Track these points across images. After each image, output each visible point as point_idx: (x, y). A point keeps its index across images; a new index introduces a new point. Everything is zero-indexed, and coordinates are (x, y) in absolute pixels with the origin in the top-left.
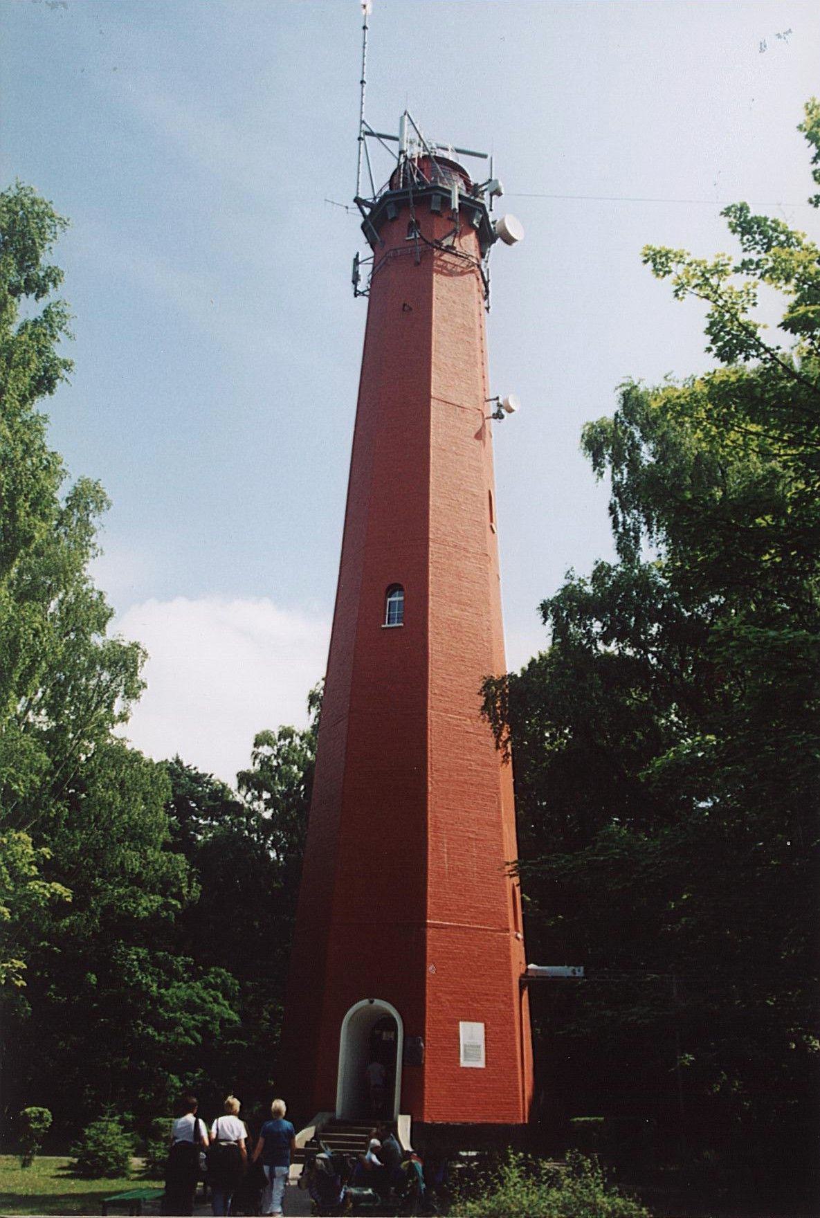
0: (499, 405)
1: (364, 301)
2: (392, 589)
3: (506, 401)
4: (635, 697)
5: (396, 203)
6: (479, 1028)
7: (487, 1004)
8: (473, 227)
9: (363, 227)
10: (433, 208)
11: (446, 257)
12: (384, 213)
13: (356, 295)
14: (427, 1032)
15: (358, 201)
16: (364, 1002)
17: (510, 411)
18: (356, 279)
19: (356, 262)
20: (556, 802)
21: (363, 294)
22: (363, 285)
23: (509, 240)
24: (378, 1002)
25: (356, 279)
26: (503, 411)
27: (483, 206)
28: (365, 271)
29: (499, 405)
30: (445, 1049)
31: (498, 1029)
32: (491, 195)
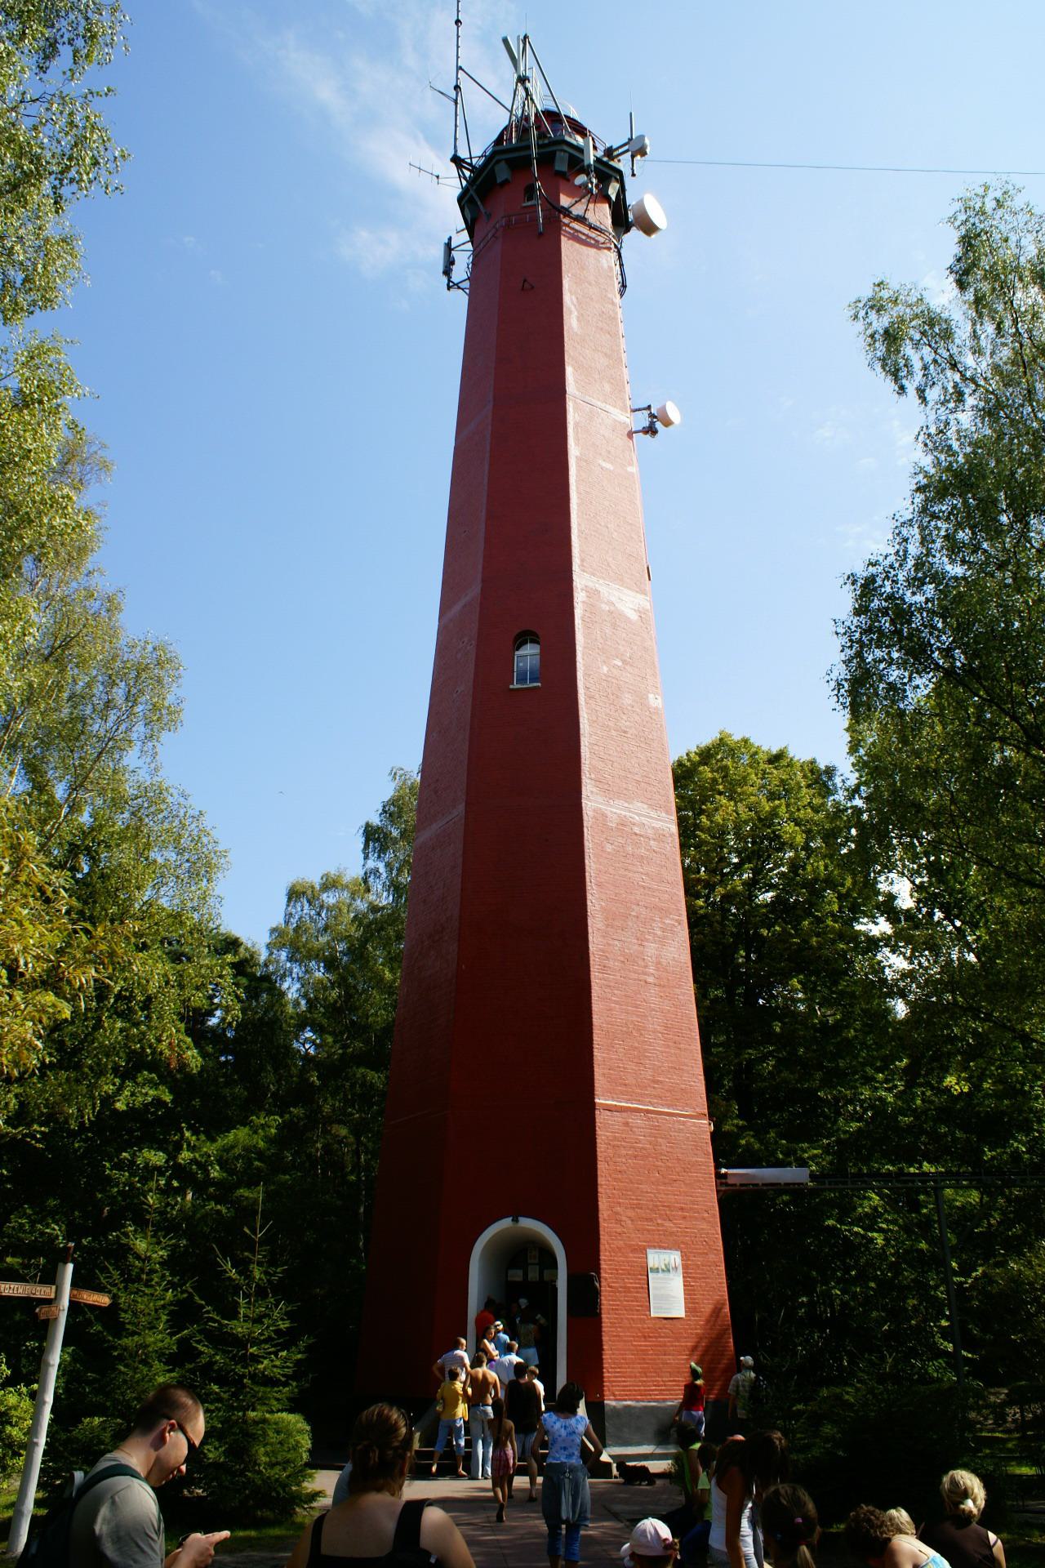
0: (652, 416)
1: (460, 301)
2: (521, 639)
3: (663, 410)
4: (882, 666)
5: (507, 161)
6: (674, 1257)
7: (683, 1224)
8: (607, 199)
9: (460, 200)
10: (557, 168)
11: (575, 225)
12: (492, 175)
13: (449, 288)
14: (603, 1266)
15: (456, 160)
16: (505, 1223)
17: (667, 423)
18: (449, 263)
19: (449, 248)
20: (760, 947)
21: (457, 286)
22: (460, 272)
23: (649, 228)
24: (528, 1224)
25: (449, 263)
26: (658, 425)
27: (620, 172)
28: (463, 261)
29: (652, 416)
30: (627, 1290)
31: (699, 1260)
32: (633, 157)
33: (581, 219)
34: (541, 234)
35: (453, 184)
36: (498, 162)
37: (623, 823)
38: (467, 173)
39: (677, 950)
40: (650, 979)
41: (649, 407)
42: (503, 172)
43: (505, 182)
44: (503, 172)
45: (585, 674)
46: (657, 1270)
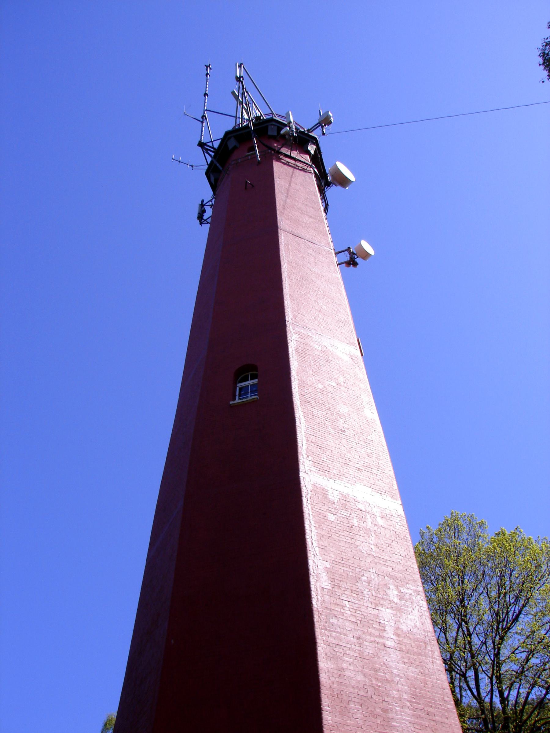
0: (350, 253)
2: (243, 372)
13: (201, 223)
15: (201, 145)
19: (202, 205)
23: (343, 181)
26: (358, 260)
27: (315, 139)
28: (209, 212)
33: (286, 156)
34: (259, 163)
35: (202, 161)
36: (230, 138)
37: (345, 500)
38: (212, 154)
39: (415, 616)
40: (389, 643)
41: (349, 248)
42: (232, 143)
43: (235, 148)
44: (232, 143)
45: (300, 386)
46: (293, 173)
